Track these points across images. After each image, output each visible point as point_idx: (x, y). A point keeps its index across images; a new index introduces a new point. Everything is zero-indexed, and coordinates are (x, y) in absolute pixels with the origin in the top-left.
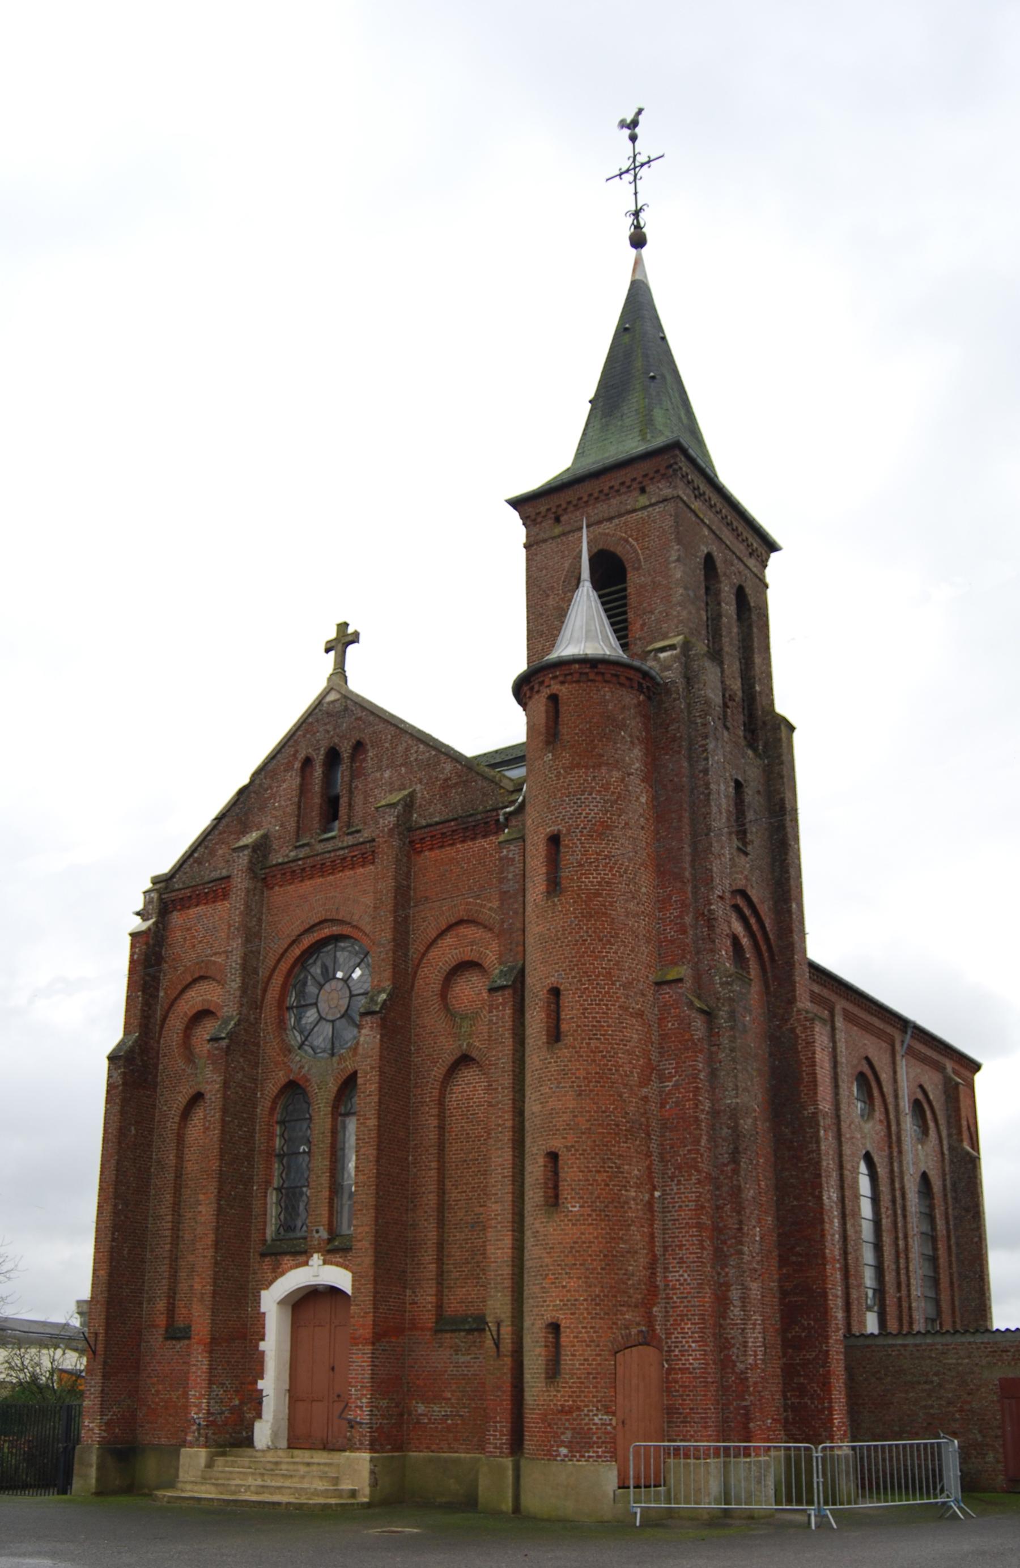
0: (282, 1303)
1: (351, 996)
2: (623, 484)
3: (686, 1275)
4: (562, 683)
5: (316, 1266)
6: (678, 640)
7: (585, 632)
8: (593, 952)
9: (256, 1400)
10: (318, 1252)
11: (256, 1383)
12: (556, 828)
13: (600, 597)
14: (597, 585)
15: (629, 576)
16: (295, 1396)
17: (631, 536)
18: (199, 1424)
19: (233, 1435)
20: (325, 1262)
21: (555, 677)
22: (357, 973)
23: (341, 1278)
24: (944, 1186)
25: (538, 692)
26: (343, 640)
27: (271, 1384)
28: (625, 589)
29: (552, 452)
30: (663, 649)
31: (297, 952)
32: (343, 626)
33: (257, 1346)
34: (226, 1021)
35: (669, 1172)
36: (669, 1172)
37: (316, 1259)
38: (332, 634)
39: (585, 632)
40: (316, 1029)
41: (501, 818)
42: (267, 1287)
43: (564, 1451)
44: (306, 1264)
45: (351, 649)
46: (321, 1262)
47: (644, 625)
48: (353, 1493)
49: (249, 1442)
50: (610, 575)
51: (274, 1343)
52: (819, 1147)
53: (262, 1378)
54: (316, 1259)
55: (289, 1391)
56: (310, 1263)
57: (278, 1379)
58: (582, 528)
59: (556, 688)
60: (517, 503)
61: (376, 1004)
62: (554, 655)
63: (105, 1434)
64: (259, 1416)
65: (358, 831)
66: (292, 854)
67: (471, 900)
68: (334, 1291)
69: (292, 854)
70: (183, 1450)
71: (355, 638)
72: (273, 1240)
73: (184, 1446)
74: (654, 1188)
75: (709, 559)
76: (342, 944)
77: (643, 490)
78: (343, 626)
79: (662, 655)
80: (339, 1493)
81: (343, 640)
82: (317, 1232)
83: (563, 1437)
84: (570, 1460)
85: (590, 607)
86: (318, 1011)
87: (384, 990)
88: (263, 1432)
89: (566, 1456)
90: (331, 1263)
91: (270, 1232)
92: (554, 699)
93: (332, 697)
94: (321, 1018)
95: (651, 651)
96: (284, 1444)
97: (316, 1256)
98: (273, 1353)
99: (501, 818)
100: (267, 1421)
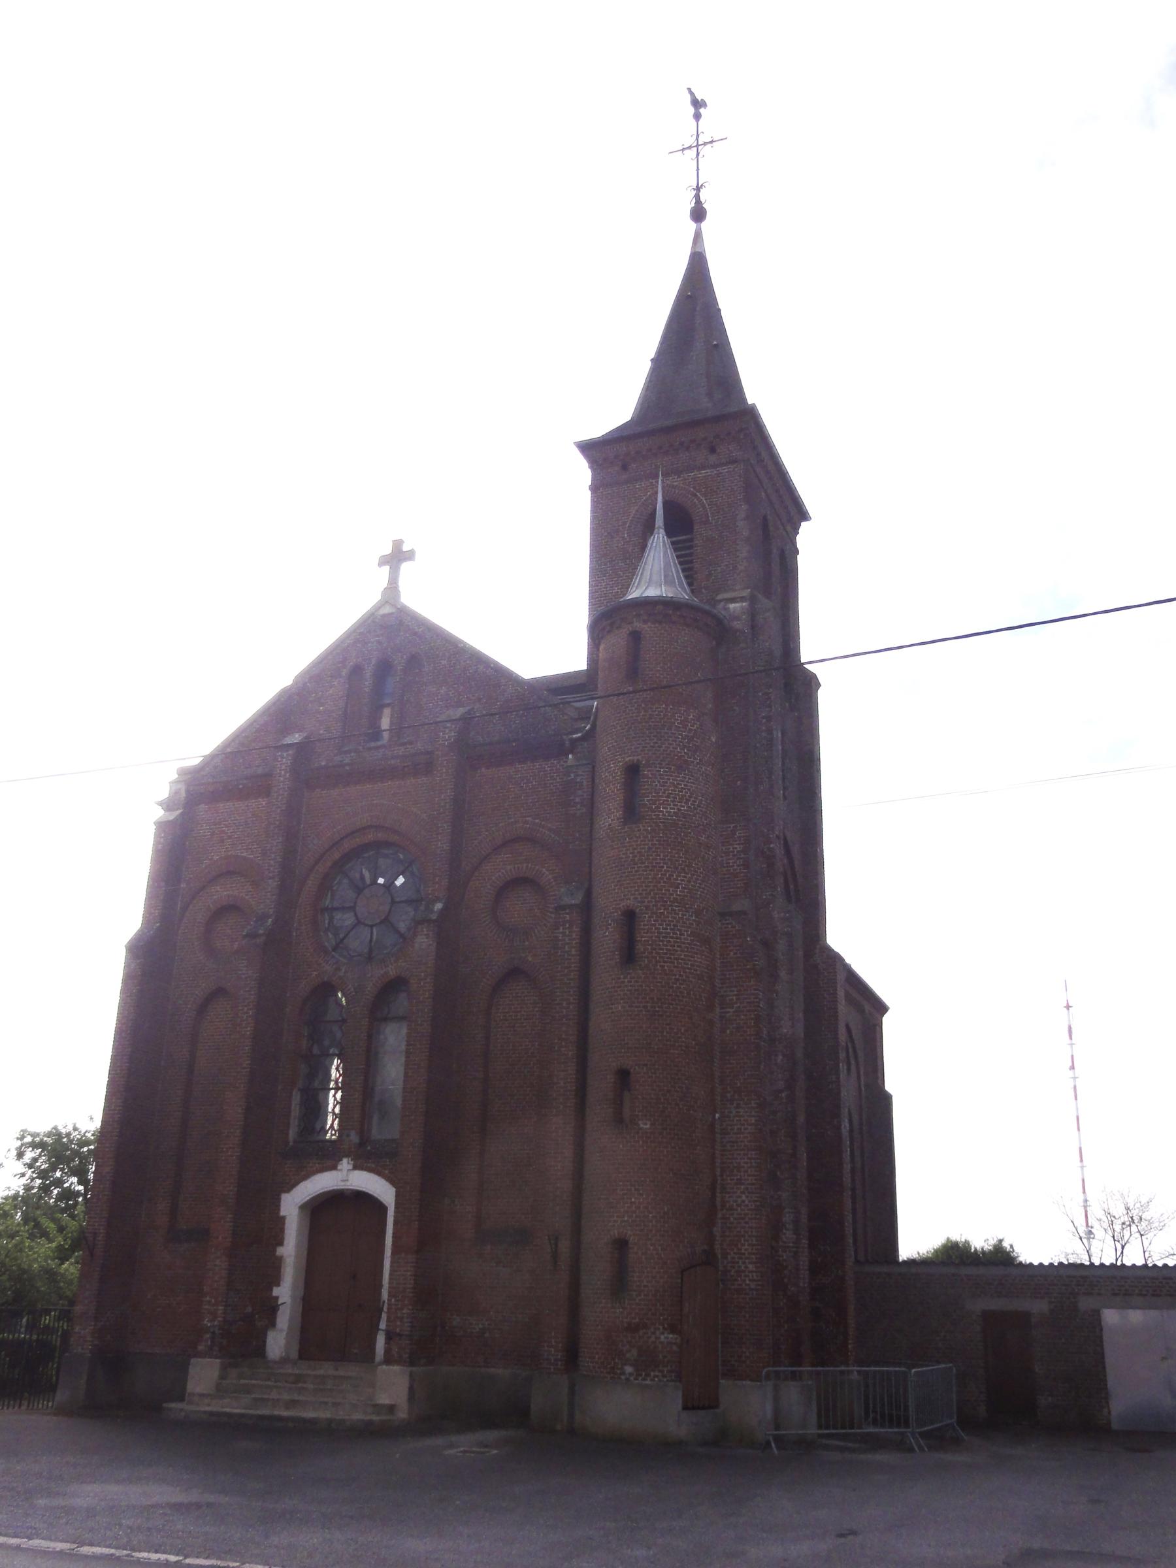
0: (303, 1207)
1: (393, 902)
2: (693, 441)
3: (744, 1197)
4: (645, 622)
5: (345, 1172)
6: (746, 593)
7: (656, 577)
8: (669, 879)
9: (272, 1308)
10: (347, 1156)
11: (271, 1290)
12: (636, 758)
13: (673, 543)
14: (670, 532)
15: (696, 527)
16: (309, 1303)
17: (699, 491)
18: (214, 1333)
19: (242, 1344)
20: (356, 1167)
21: (638, 615)
22: (400, 881)
23: (380, 1188)
24: (861, 1119)
25: (619, 627)
26: (397, 557)
27: (285, 1292)
28: (691, 540)
29: (616, 403)
30: (733, 600)
31: (337, 856)
32: (398, 544)
33: (275, 1251)
34: (263, 918)
35: (729, 1095)
36: (729, 1095)
37: (345, 1164)
38: (388, 550)
39: (656, 577)
40: (352, 933)
41: (567, 744)
42: (288, 1191)
43: (629, 1369)
44: (334, 1168)
45: (405, 567)
46: (351, 1167)
47: (710, 574)
48: (391, 1409)
49: (261, 1351)
50: (680, 523)
51: (291, 1248)
52: (838, 1078)
53: (278, 1285)
54: (345, 1164)
55: (304, 1299)
56: (339, 1167)
57: (294, 1287)
58: (657, 476)
59: (637, 625)
60: (589, 448)
61: (432, 911)
62: (634, 594)
63: (96, 1343)
64: (272, 1324)
65: (411, 743)
66: (338, 758)
67: (529, 819)
68: (362, 1198)
69: (338, 758)
70: (193, 1361)
71: (410, 556)
72: (295, 1142)
73: (195, 1356)
74: (716, 1112)
75: (765, 519)
76: (386, 851)
77: (713, 450)
78: (398, 544)
79: (732, 606)
80: (378, 1408)
81: (397, 557)
82: (348, 1136)
83: (628, 1355)
84: (636, 1379)
85: (665, 553)
86: (356, 915)
87: (437, 899)
88: (278, 1342)
89: (631, 1374)
90: (362, 1169)
91: (292, 1134)
92: (636, 637)
93: (387, 610)
94: (359, 922)
95: (721, 601)
96: (294, 1355)
97: (345, 1161)
98: (292, 1259)
99: (567, 744)
100: (281, 1330)
